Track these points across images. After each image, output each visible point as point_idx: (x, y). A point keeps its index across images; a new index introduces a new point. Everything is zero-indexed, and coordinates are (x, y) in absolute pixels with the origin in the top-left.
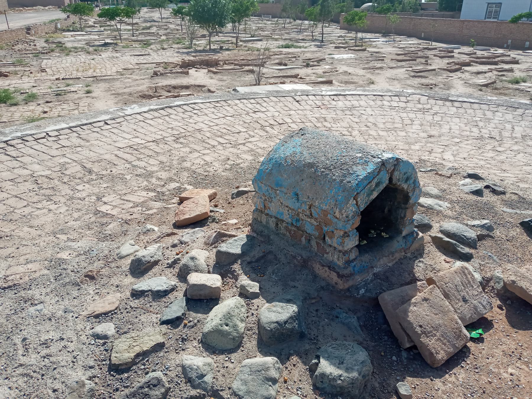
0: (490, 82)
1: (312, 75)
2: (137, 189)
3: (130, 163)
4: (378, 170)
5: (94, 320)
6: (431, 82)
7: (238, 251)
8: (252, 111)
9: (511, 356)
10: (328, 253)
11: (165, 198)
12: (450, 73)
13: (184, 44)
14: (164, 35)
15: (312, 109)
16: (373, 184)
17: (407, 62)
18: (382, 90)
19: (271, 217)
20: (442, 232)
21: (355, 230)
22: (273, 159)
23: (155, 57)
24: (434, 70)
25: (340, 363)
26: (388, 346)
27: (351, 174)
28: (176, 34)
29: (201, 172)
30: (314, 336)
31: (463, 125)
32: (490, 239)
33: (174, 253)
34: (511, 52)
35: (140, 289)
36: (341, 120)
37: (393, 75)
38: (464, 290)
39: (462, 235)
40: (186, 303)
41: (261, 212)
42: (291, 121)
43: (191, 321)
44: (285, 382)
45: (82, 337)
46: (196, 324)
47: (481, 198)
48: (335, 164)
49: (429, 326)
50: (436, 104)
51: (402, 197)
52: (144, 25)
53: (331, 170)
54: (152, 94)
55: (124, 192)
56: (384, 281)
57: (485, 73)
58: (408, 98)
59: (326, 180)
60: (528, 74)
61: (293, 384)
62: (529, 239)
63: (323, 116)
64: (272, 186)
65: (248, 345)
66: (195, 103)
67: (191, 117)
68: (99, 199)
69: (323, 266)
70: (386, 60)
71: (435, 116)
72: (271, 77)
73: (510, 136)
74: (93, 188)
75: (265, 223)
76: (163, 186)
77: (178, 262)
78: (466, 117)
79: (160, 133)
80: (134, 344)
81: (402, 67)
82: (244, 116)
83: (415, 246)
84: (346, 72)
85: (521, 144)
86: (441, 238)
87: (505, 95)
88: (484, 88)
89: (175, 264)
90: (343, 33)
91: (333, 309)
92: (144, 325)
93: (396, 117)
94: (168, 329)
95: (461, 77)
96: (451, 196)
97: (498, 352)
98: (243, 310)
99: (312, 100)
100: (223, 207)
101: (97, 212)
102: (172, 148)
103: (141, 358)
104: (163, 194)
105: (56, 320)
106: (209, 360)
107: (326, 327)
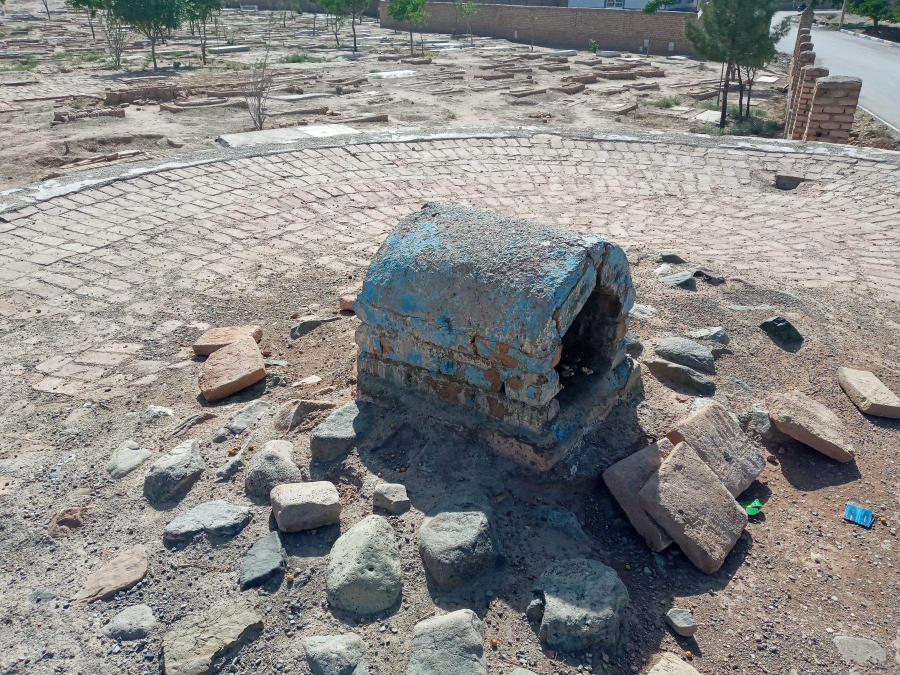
0: (629, 106)
1: (350, 107)
2: (102, 340)
3: (72, 292)
4: (583, 266)
5: (105, 605)
6: (543, 111)
7: (348, 432)
8: (279, 177)
9: (807, 533)
10: (511, 414)
11: (163, 350)
12: (569, 96)
13: (104, 61)
14: (59, 45)
15: (381, 166)
16: (578, 289)
17: (501, 80)
18: (488, 128)
19: (396, 364)
20: (659, 353)
21: (554, 371)
22: (390, 262)
23: (52, 86)
24: (544, 91)
25: (578, 597)
26: (632, 553)
27: (541, 276)
28: (84, 42)
29: (216, 296)
30: (518, 559)
31: (624, 179)
32: (727, 355)
33: (224, 452)
34: (650, 59)
35: (183, 530)
36: (435, 184)
37: (482, 102)
38: (724, 442)
39: (692, 355)
40: (282, 541)
41: (376, 357)
42: (353, 191)
43: (299, 574)
44: (495, 647)
45: (90, 644)
46: (309, 577)
47: (694, 293)
48: (510, 262)
49: (692, 508)
50: (575, 148)
51: (607, 305)
52: (14, 26)
53: (504, 273)
54: (60, 157)
55: (77, 348)
56: (601, 447)
57: (620, 92)
58: (532, 141)
59: (499, 290)
60: (680, 93)
61: (508, 648)
62: (778, 348)
63: (403, 178)
64: (396, 310)
65: (413, 596)
66: (168, 170)
67: (167, 195)
68: (29, 368)
69: (506, 437)
70: (466, 79)
71: (579, 167)
72: (280, 115)
73: (695, 190)
74: (11, 348)
75: (384, 377)
76: (152, 329)
77: (239, 468)
78: (625, 165)
79: (116, 229)
80: (205, 636)
81: (494, 88)
82: (265, 186)
83: (632, 381)
84: (406, 101)
85: (714, 202)
86: (666, 364)
87: (654, 126)
88: (622, 117)
89: (235, 473)
90: (386, 33)
91: (533, 506)
92: (210, 597)
93: (521, 173)
94: (260, 595)
95: (586, 101)
96: (651, 295)
97: (789, 531)
98: (391, 536)
99: (379, 152)
100: (280, 355)
101: (34, 395)
102: (146, 256)
103: (224, 659)
104: (156, 343)
105: (21, 621)
106: (352, 637)
107: (531, 539)
